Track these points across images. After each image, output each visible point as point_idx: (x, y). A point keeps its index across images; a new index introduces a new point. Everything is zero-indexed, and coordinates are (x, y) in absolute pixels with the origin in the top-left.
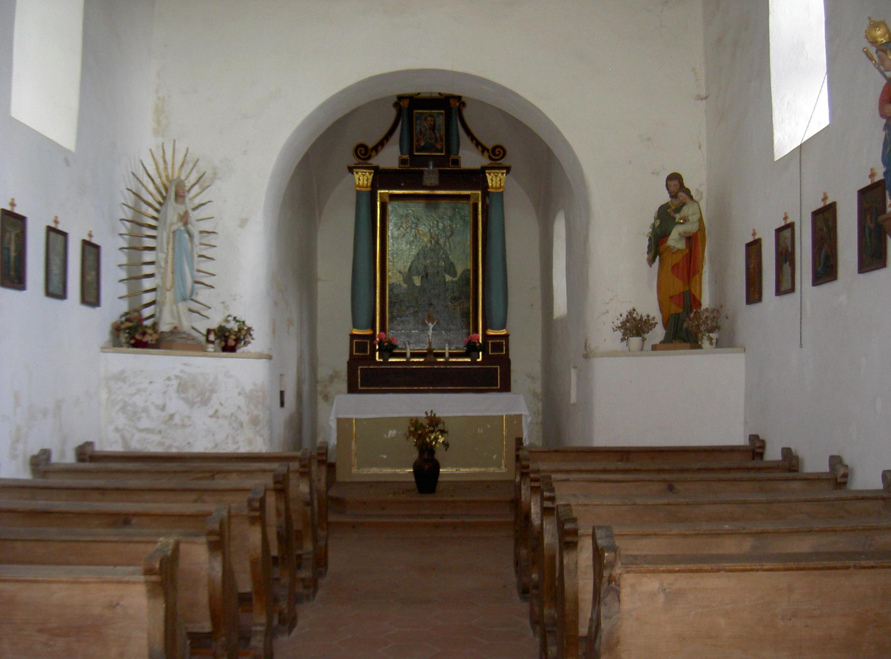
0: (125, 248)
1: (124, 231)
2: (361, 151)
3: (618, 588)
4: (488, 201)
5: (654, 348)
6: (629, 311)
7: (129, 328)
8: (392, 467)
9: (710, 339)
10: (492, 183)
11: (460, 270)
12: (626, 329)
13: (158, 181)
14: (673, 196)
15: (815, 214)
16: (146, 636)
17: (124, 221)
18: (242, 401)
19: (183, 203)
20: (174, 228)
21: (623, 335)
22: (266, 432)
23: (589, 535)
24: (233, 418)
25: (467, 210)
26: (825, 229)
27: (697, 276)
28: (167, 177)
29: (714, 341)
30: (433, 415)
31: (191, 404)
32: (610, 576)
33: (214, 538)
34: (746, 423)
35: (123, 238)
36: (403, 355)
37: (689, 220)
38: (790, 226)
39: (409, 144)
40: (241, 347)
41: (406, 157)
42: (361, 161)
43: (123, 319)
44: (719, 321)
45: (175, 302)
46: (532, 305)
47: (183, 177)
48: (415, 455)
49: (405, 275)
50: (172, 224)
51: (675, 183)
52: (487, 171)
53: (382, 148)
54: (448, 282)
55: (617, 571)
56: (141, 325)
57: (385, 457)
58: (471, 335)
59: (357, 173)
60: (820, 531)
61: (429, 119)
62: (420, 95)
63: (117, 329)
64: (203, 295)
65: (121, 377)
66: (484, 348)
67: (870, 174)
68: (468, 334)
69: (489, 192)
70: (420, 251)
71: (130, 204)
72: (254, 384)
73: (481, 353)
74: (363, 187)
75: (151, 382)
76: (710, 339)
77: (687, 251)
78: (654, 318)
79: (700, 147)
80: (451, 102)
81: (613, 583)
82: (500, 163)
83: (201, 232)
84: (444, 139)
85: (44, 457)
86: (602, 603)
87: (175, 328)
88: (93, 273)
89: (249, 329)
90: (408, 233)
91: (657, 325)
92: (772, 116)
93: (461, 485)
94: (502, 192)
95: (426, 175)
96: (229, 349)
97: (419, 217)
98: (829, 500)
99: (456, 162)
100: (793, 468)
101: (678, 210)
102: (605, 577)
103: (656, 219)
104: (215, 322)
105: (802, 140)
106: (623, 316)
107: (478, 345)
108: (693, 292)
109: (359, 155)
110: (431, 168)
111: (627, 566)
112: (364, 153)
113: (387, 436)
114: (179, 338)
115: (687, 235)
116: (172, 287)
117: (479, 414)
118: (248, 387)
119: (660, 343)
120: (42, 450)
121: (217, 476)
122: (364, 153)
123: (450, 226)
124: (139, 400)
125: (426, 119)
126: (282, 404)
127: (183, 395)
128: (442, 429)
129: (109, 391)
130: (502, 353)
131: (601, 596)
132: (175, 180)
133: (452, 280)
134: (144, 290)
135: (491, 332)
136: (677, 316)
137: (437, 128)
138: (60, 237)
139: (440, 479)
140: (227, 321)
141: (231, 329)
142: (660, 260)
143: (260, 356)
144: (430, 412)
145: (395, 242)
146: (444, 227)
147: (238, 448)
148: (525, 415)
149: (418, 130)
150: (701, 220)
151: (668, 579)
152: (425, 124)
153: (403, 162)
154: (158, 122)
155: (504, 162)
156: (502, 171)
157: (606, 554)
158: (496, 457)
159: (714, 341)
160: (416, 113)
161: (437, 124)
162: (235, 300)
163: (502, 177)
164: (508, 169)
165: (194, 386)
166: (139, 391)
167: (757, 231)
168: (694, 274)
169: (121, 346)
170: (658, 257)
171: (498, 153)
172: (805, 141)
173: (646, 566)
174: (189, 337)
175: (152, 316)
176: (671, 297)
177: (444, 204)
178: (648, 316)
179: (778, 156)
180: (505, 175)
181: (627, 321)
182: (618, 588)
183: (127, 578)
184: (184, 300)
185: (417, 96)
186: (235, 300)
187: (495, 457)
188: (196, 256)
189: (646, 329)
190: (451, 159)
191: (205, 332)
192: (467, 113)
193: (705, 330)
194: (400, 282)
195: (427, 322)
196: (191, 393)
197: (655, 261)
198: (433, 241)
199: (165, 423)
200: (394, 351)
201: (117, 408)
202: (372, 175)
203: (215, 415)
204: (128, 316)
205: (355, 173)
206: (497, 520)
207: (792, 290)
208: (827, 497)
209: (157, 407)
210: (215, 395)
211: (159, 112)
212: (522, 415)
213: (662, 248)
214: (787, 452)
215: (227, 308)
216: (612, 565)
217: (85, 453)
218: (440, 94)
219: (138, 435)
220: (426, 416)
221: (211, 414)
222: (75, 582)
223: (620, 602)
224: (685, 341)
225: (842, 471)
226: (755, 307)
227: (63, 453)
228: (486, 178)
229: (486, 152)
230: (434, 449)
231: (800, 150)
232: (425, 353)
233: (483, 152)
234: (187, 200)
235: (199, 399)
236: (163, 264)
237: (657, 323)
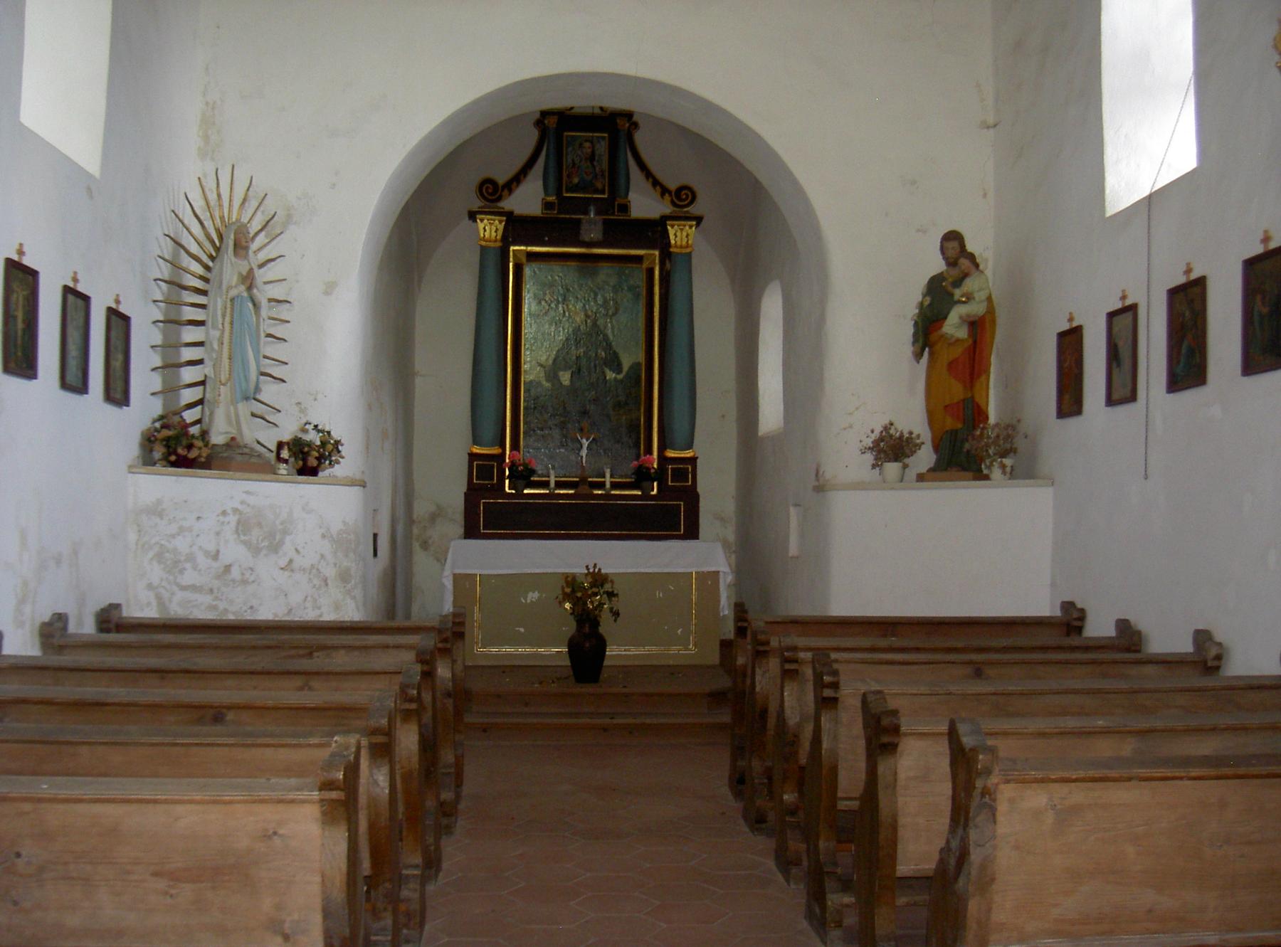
0: (161, 322)
1: (159, 297)
2: (487, 188)
3: (993, 804)
4: (668, 265)
5: (921, 478)
6: (883, 425)
7: (168, 439)
8: (532, 645)
9: (1003, 467)
10: (675, 240)
11: (626, 363)
12: (879, 452)
13: (208, 224)
14: (951, 263)
15: (1173, 293)
16: (318, 879)
17: (159, 282)
18: (326, 547)
19: (246, 257)
20: (233, 293)
21: (876, 459)
22: (358, 593)
23: (941, 734)
24: (314, 571)
25: (639, 279)
26: (1187, 314)
27: (983, 378)
28: (222, 218)
29: (1008, 469)
30: (596, 570)
31: (256, 550)
32: (985, 787)
33: (380, 739)
34: (1053, 585)
35: (157, 305)
36: (545, 485)
37: (974, 298)
38: (1131, 310)
39: (556, 181)
40: (326, 468)
41: (552, 199)
42: (487, 203)
43: (158, 425)
44: (1014, 441)
45: (234, 402)
46: (723, 416)
47: (245, 220)
48: (570, 628)
49: (546, 369)
50: (230, 288)
51: (954, 244)
52: (668, 222)
53: (518, 185)
54: (610, 379)
55: (993, 779)
56: (186, 434)
57: (522, 630)
58: (643, 458)
59: (482, 220)
60: (1262, 728)
61: (587, 144)
62: (573, 111)
63: (149, 440)
64: (269, 392)
65: (156, 510)
66: (660, 475)
67: (1262, 237)
68: (638, 456)
69: (670, 253)
70: (569, 335)
71: (167, 257)
72: (344, 523)
73: (655, 484)
74: (490, 242)
75: (199, 518)
76: (1003, 467)
77: (970, 342)
78: (918, 436)
79: (985, 195)
80: (618, 121)
81: (987, 796)
82: (687, 212)
83: (270, 300)
84: (607, 174)
85: (59, 625)
86: (971, 824)
87: (233, 439)
88: (120, 357)
89: (337, 443)
90: (552, 308)
91: (923, 446)
92: (1103, 154)
93: (630, 671)
94: (691, 253)
95: (584, 227)
96: (308, 472)
97: (569, 287)
98: (1214, 690)
99: (625, 208)
100: (1133, 648)
101: (958, 283)
102: (978, 788)
103: (924, 296)
104: (287, 432)
105: (1152, 189)
106: (875, 432)
107: (652, 471)
108: (977, 399)
109: (486, 194)
110: (592, 216)
111: (1007, 773)
112: (491, 192)
113: (526, 601)
114: (240, 454)
115: (972, 319)
116: (229, 379)
117: (656, 570)
118: (336, 527)
119: (928, 471)
120: (54, 614)
121: (316, 654)
122: (491, 192)
123: (613, 300)
124: (182, 544)
125: (581, 145)
126: (375, 554)
127: (243, 538)
128: (610, 590)
129: (139, 531)
130: (687, 484)
131: (971, 815)
132: (234, 223)
133: (615, 378)
134: (182, 384)
135: (671, 454)
136: (954, 433)
137: (596, 158)
138: (80, 302)
139: (606, 663)
140: (304, 431)
141: (311, 441)
142: (931, 354)
143: (352, 483)
144: (593, 565)
145: (533, 322)
146: (605, 301)
147: (321, 616)
148: (724, 573)
149: (570, 160)
150: (989, 299)
151: (1061, 790)
152: (579, 153)
153: (547, 206)
154: (206, 138)
155: (694, 210)
156: (689, 223)
157: (981, 757)
158: (681, 632)
159: (1008, 469)
160: (567, 136)
161: (597, 153)
162: (315, 399)
163: (690, 231)
164: (699, 220)
165: (259, 525)
166: (181, 530)
167: (1075, 315)
168: (979, 375)
169: (154, 464)
170: (927, 349)
171: (684, 197)
172: (1159, 190)
173: (1033, 773)
174: (252, 453)
175: (198, 422)
176: (946, 407)
177: (606, 271)
178: (911, 433)
179: (1111, 210)
180: (694, 228)
181: (881, 439)
182: (993, 804)
183: (291, 796)
184: (247, 398)
185: (568, 112)
186: (315, 399)
187: (679, 631)
188: (263, 335)
189: (907, 451)
190: (616, 203)
191: (274, 448)
192: (639, 137)
193: (995, 454)
194: (541, 379)
195: (579, 438)
196: (256, 534)
197: (922, 355)
198: (589, 321)
199: (218, 577)
200: (532, 479)
201: (151, 554)
202: (504, 223)
203: (289, 567)
204: (165, 421)
205: (478, 221)
206: (690, 720)
207: (1133, 397)
208: (1210, 685)
209: (207, 554)
210: (288, 539)
211: (208, 122)
212: (719, 572)
213: (933, 337)
214: (1124, 626)
215: (303, 411)
216: (988, 772)
217: (109, 620)
218: (601, 108)
219: (180, 595)
220: (586, 572)
221: (283, 566)
222: (215, 802)
223: (995, 822)
224: (964, 469)
225: (1213, 652)
226: (1072, 422)
227: (80, 623)
228: (666, 231)
229: (667, 195)
230: (598, 618)
231: (1149, 202)
232: (576, 481)
233: (663, 195)
234: (251, 252)
235: (266, 543)
236: (216, 346)
237: (923, 443)
